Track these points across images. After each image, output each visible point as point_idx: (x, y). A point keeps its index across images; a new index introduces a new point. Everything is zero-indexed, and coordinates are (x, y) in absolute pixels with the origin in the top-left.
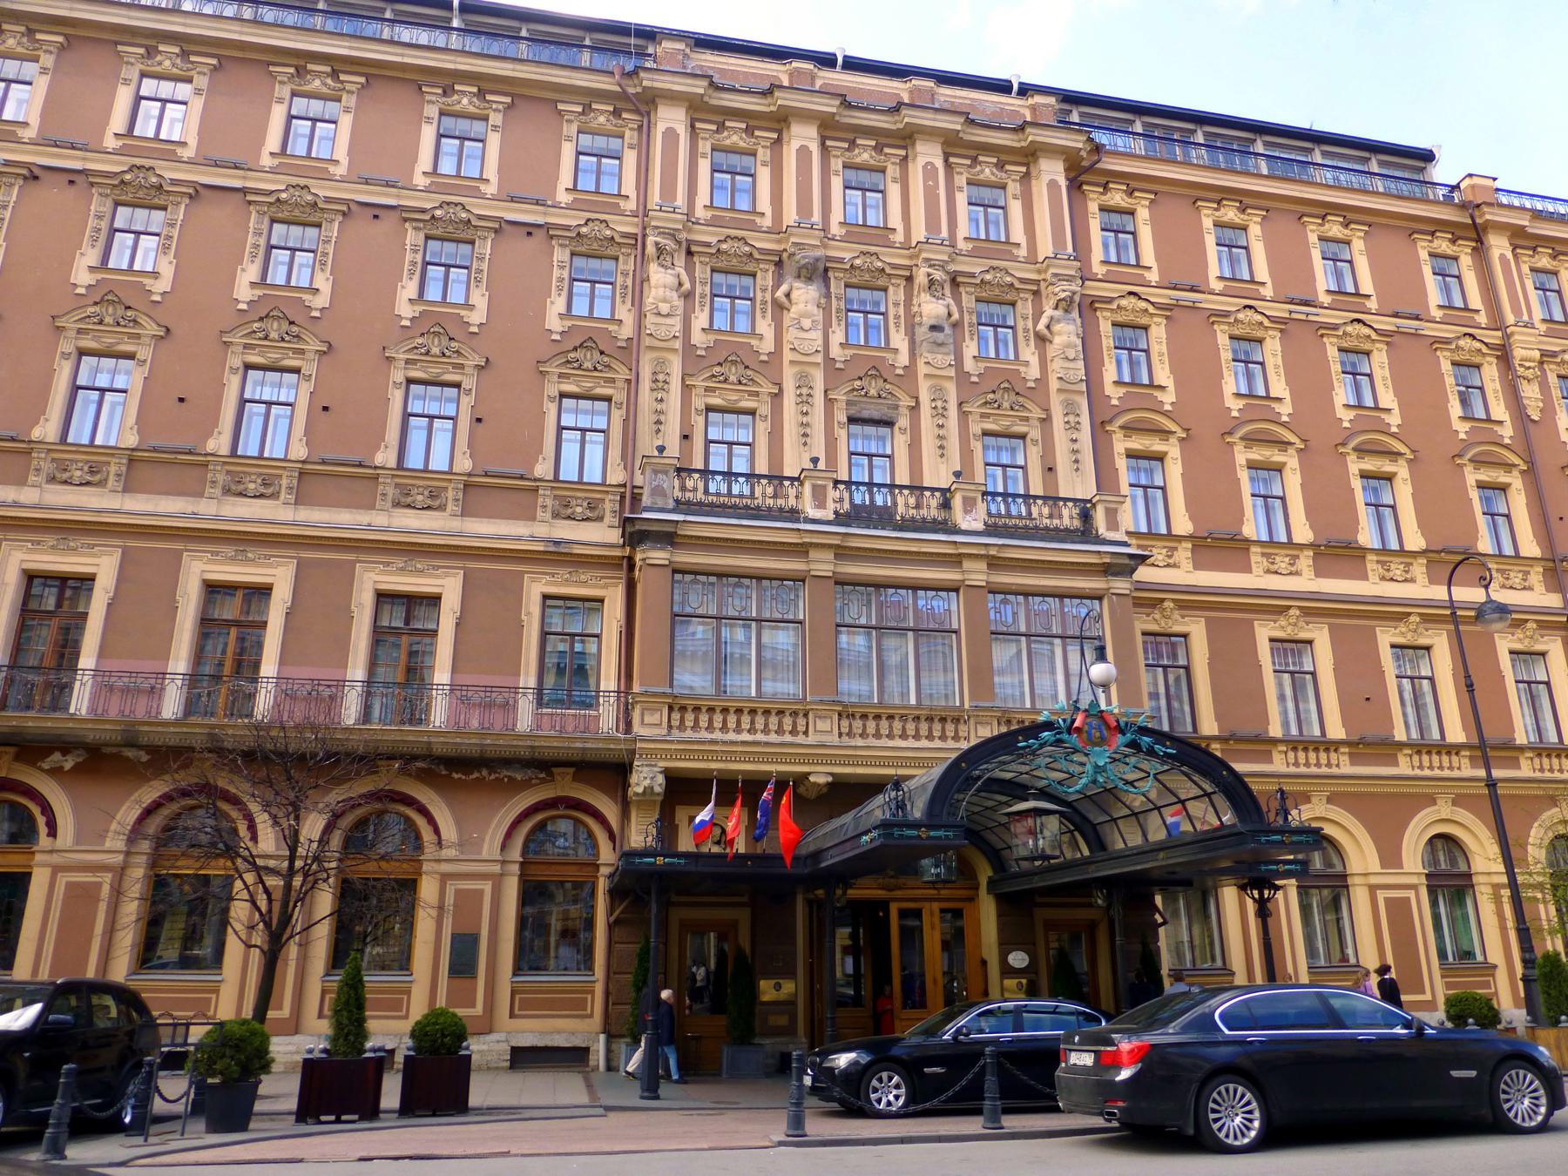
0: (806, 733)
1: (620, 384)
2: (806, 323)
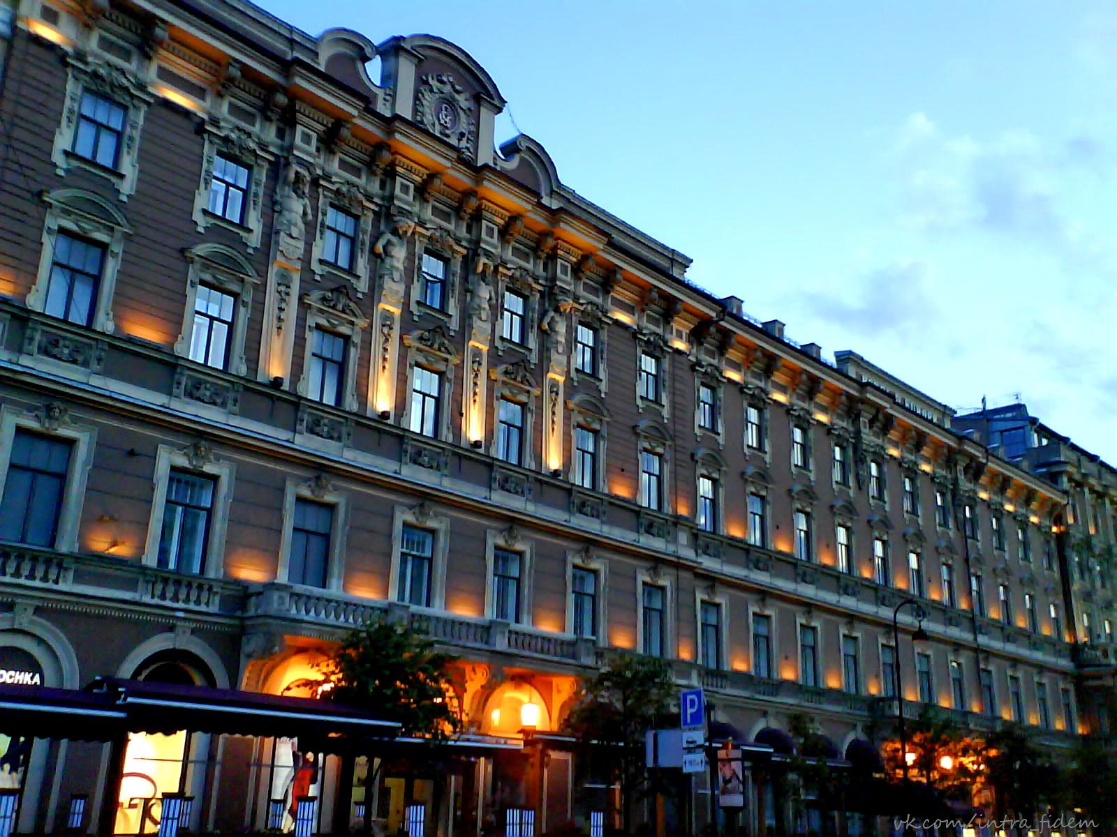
0: (56, 582)
1: (118, 235)
2: (295, 233)
